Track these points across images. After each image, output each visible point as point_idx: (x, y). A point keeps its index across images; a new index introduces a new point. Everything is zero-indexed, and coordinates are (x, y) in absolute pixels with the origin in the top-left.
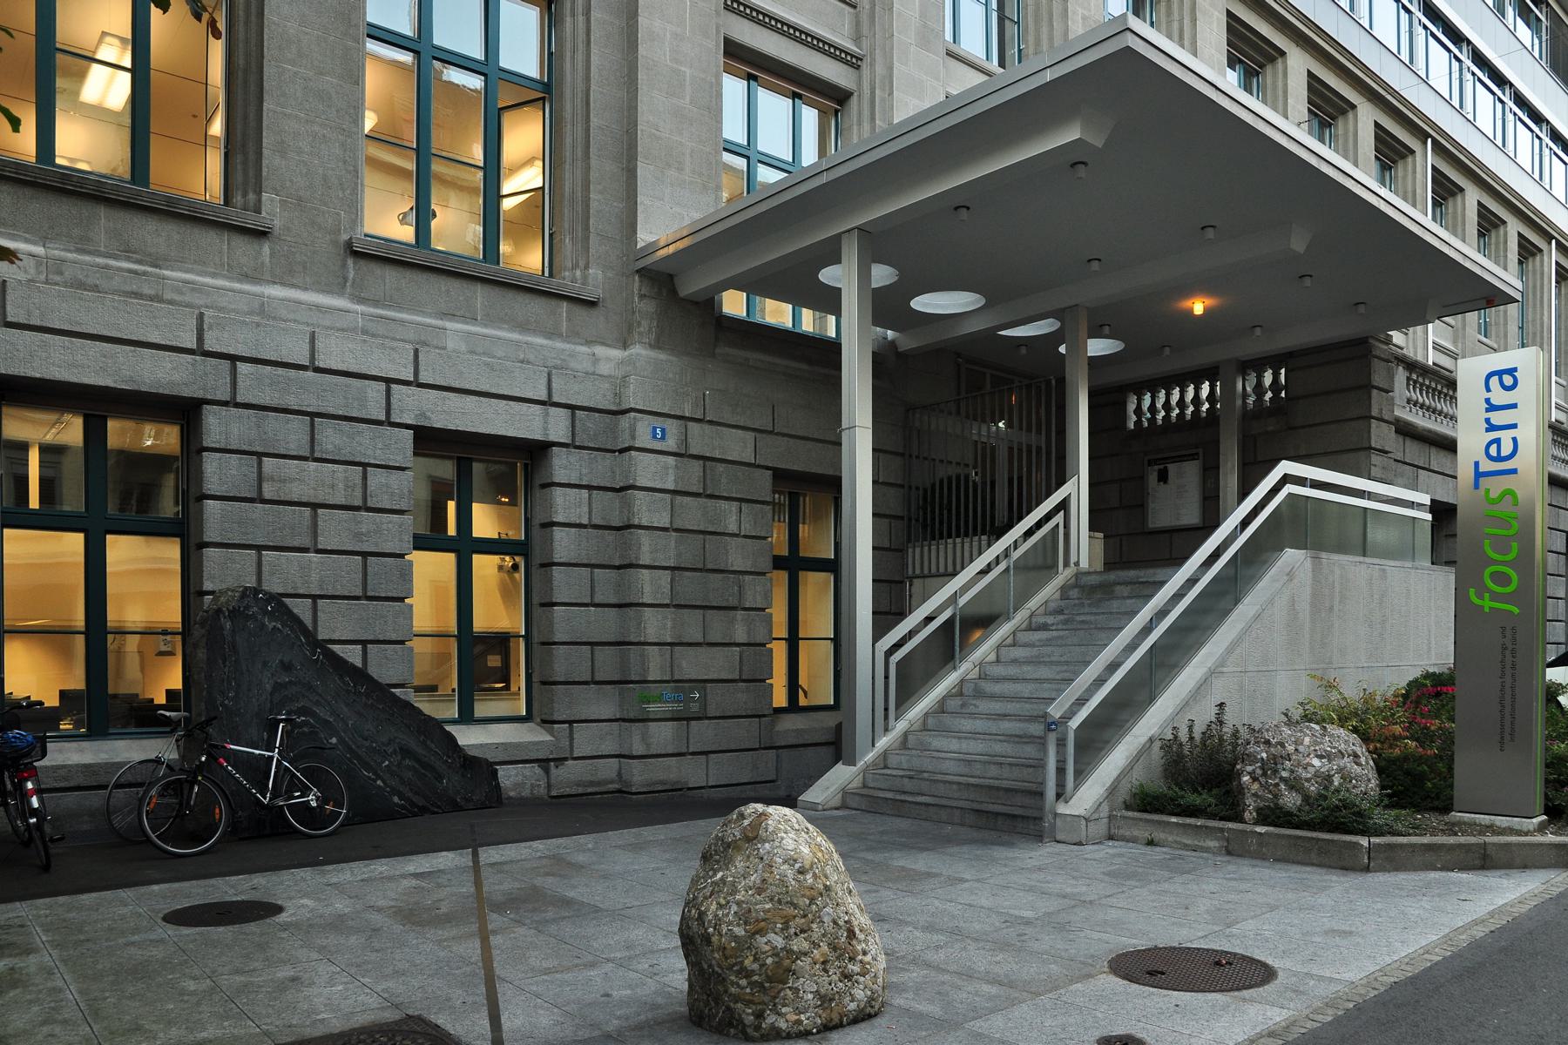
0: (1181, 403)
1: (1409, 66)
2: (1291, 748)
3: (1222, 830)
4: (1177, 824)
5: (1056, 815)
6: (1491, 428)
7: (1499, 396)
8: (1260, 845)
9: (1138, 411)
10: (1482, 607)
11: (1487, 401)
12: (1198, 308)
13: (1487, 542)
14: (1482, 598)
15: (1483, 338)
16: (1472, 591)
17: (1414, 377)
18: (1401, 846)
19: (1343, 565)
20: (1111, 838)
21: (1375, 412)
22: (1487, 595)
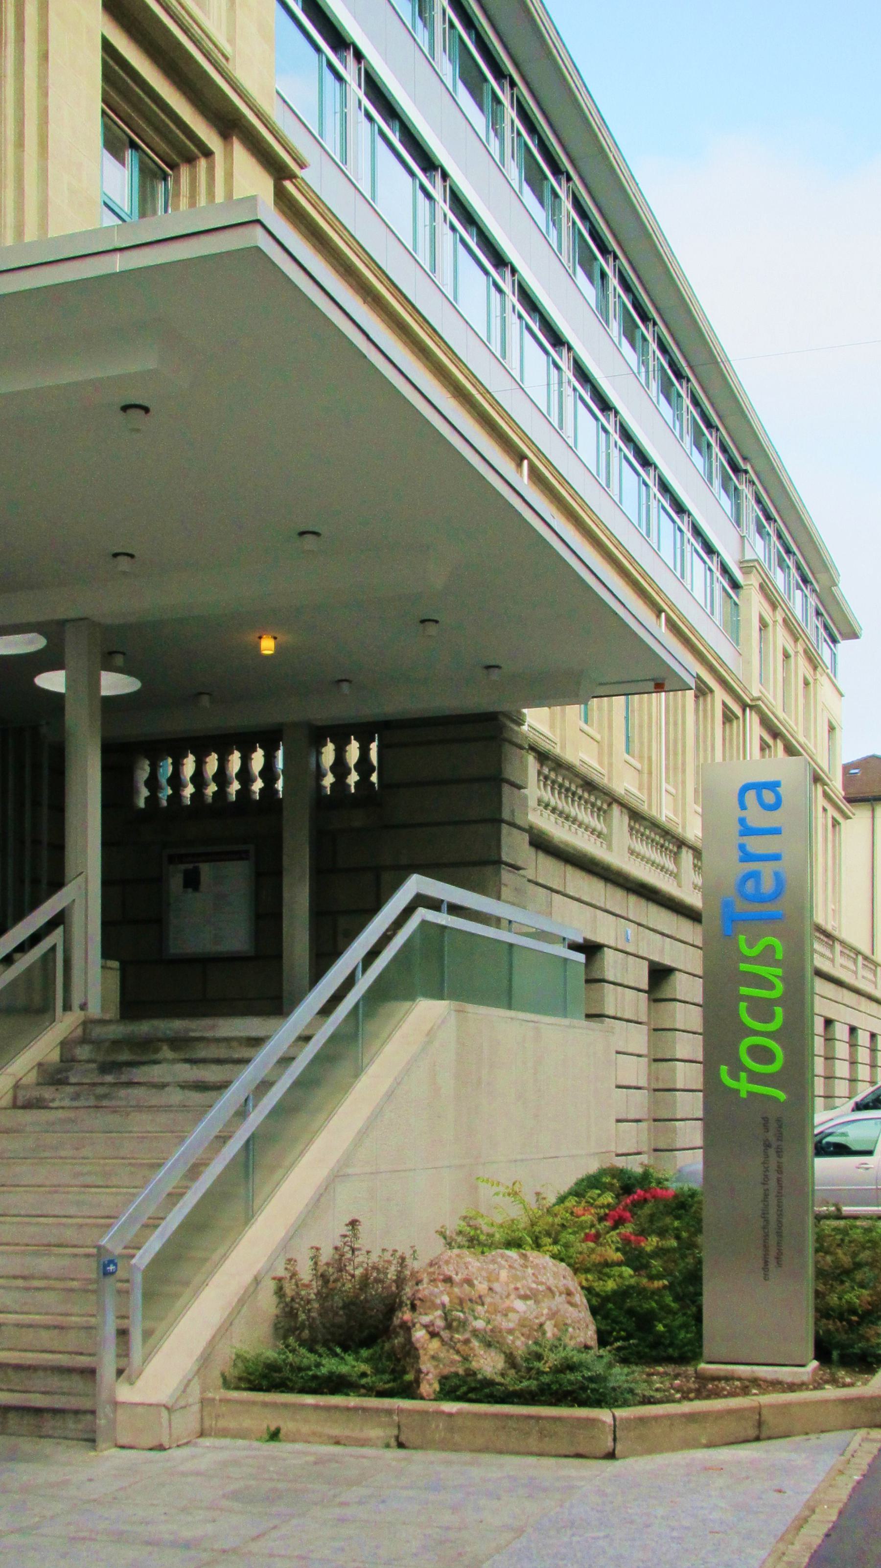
0: (221, 777)
1: (500, 360)
2: (482, 1287)
3: (389, 1412)
4: (316, 1407)
5: (116, 1404)
6: (746, 857)
7: (756, 817)
8: (451, 1430)
9: (153, 783)
10: (737, 1091)
11: (742, 821)
12: (268, 646)
13: (743, 1006)
14: (736, 1078)
15: (585, 727)
16: (724, 1069)
17: (546, 771)
18: (656, 1418)
19: (503, 1027)
20: (202, 1434)
21: (506, 815)
22: (743, 1075)
